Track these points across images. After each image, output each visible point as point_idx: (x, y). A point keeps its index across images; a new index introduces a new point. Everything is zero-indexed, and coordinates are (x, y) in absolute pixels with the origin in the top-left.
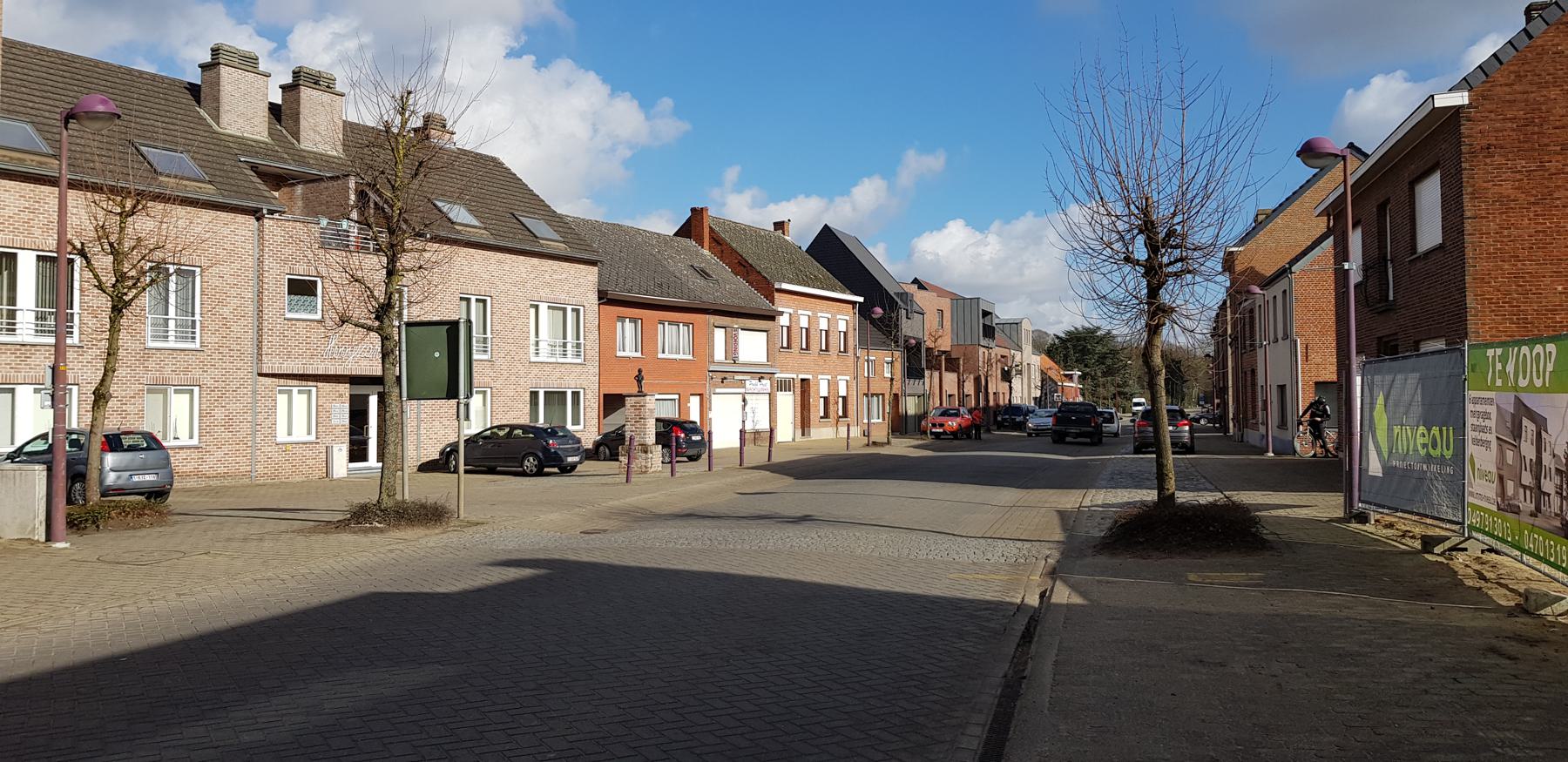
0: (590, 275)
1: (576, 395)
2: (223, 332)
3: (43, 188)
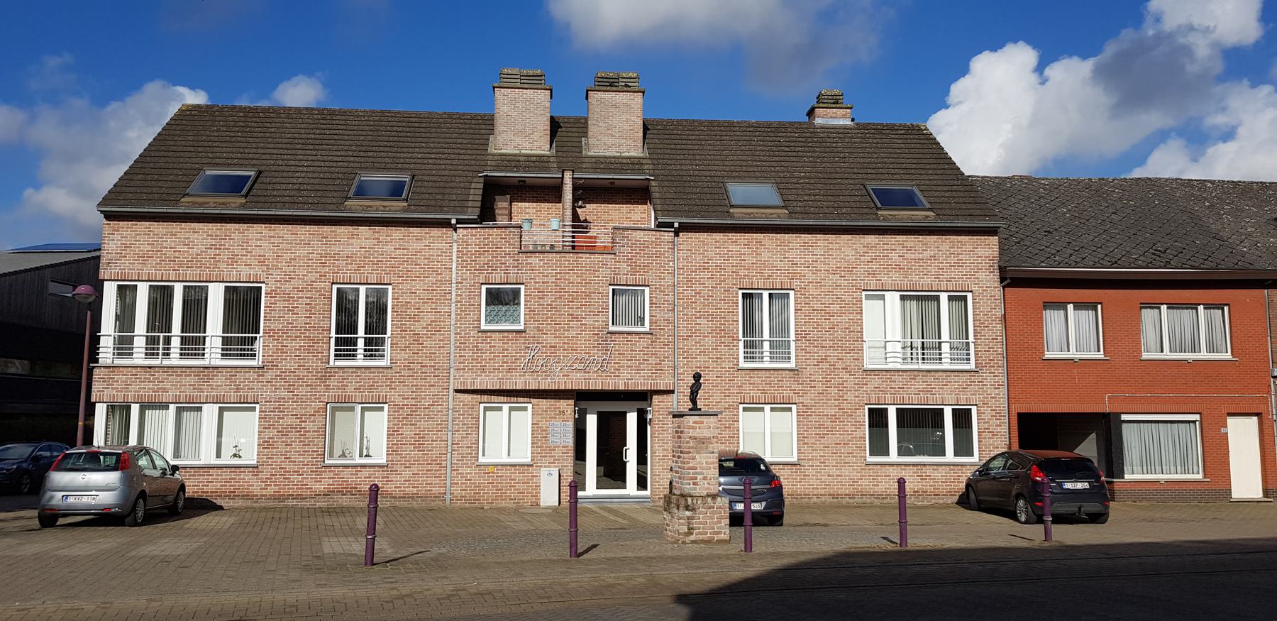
0: (988, 248)
1: (962, 418)
2: (415, 347)
3: (229, 225)
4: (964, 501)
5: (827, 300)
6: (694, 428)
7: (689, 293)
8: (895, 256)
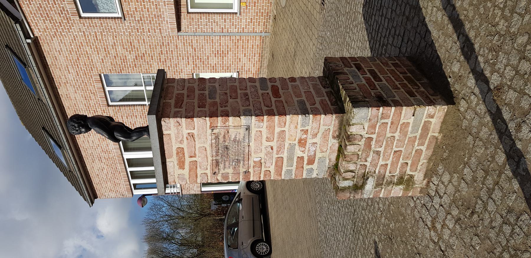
6: (194, 165)
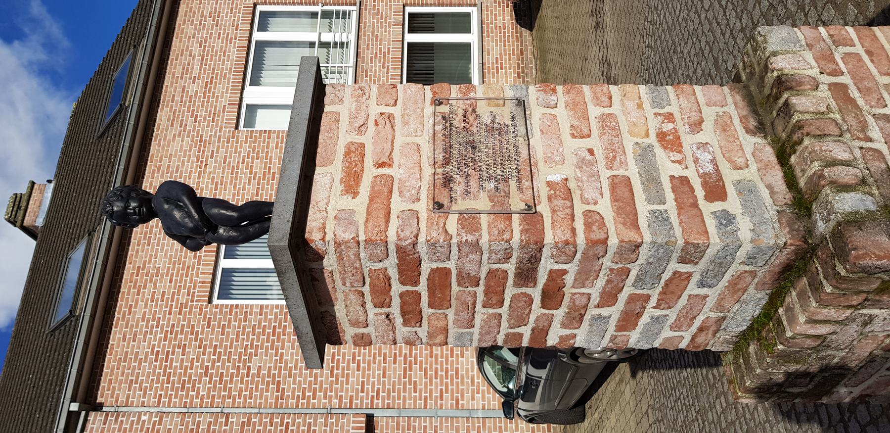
1: (417, 23)
4: (531, 28)
5: (244, 176)
6: (383, 192)
7: (203, 387)
8: (192, 88)
